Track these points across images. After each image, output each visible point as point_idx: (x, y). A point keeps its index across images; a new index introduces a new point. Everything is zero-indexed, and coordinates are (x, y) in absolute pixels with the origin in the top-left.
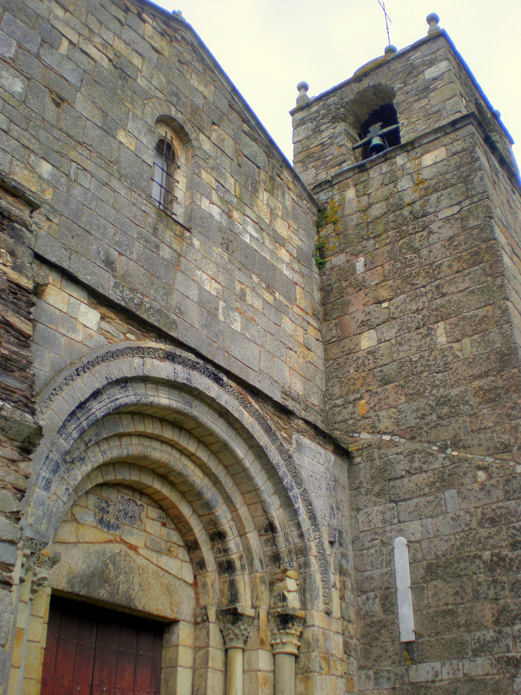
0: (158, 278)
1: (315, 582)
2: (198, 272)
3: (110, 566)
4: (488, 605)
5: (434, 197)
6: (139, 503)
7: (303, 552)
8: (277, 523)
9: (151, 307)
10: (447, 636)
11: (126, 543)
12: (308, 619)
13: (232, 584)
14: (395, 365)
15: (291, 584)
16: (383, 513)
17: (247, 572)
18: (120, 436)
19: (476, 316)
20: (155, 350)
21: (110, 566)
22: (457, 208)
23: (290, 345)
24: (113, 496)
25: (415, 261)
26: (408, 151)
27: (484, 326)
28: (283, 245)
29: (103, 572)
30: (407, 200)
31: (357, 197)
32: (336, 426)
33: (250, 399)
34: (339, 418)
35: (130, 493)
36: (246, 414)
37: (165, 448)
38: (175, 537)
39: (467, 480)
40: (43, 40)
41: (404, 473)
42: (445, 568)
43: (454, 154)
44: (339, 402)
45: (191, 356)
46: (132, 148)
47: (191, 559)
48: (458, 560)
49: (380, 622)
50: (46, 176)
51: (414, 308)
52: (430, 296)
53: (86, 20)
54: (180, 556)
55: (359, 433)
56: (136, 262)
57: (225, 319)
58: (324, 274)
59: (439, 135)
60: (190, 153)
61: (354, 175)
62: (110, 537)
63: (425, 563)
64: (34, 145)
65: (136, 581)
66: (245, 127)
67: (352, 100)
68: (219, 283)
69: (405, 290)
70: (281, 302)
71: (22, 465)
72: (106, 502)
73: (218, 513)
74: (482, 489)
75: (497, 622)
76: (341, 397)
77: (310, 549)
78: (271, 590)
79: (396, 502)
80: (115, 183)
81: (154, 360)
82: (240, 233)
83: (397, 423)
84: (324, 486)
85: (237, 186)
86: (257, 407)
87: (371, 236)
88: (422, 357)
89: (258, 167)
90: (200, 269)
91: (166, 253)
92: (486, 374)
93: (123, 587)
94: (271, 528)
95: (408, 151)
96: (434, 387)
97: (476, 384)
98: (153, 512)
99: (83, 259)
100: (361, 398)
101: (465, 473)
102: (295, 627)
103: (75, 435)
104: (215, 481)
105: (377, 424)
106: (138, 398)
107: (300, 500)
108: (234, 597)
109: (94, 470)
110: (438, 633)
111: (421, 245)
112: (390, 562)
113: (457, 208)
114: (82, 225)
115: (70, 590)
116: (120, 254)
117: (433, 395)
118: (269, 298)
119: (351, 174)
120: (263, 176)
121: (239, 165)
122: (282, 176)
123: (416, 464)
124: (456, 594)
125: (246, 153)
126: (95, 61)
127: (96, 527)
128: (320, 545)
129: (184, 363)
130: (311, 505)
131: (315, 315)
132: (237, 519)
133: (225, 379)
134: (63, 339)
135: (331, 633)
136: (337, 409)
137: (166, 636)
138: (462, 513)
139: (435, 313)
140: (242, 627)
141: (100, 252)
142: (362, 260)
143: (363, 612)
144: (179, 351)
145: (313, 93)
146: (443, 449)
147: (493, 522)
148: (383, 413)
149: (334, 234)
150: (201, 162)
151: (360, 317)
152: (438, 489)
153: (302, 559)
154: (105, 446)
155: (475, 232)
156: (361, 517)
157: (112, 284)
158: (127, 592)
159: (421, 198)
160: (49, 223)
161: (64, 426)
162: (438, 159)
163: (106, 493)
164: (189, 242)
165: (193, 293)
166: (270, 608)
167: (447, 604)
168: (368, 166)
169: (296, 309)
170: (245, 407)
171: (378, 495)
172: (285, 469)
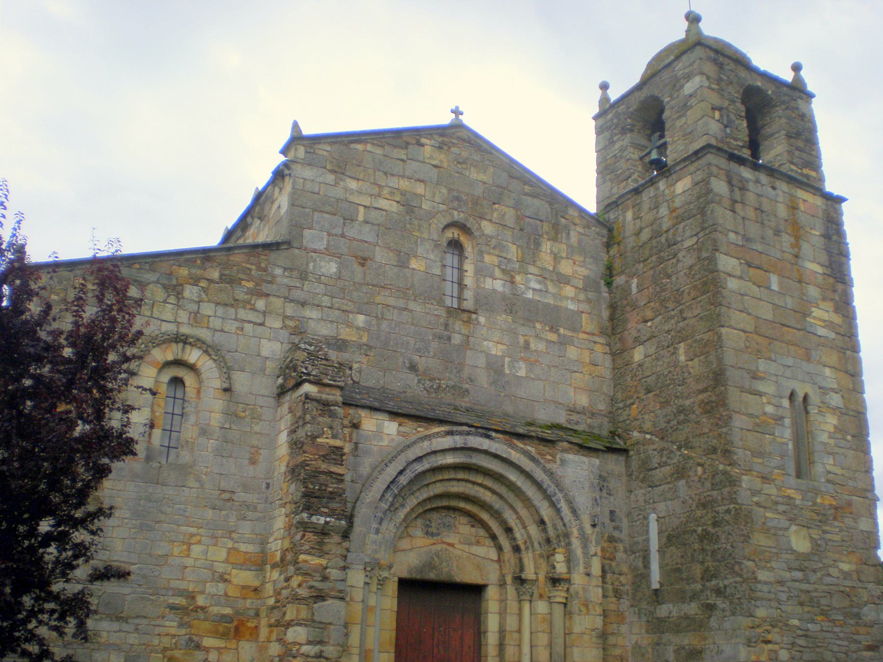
0: (451, 362)
1: (576, 555)
2: (485, 343)
3: (436, 559)
4: (699, 566)
5: (681, 226)
6: (453, 516)
7: (567, 535)
8: (546, 519)
9: (447, 386)
10: (677, 587)
11: (445, 543)
12: (572, 580)
13: (521, 560)
14: (654, 377)
15: (559, 557)
16: (645, 495)
17: (531, 551)
18: (428, 485)
19: (703, 339)
20: (438, 433)
21: (436, 559)
22: (695, 239)
23: (575, 369)
24: (435, 516)
25: (668, 286)
26: (667, 177)
27: (707, 349)
28: (568, 283)
29: (431, 563)
30: (664, 228)
31: (634, 219)
32: (619, 425)
33: (515, 441)
34: (621, 419)
35: (446, 511)
36: (513, 452)
37: (460, 483)
38: (482, 532)
39: (691, 473)
40: (345, 219)
41: (657, 465)
42: (677, 538)
43: (697, 184)
44: (621, 405)
45: (465, 428)
46: (422, 269)
47: (495, 545)
48: (685, 532)
49: (641, 574)
50: (361, 325)
51: (666, 328)
52: (676, 318)
53: (374, 180)
54: (487, 544)
55: (633, 431)
56: (433, 357)
57: (511, 371)
58: (612, 293)
59: (687, 163)
60: (474, 241)
61: (632, 196)
62: (433, 541)
63: (666, 533)
64: (350, 306)
65: (454, 565)
66: (527, 189)
67: (635, 110)
68: (504, 344)
69: (662, 312)
70: (565, 336)
71: (344, 544)
72: (429, 520)
73: (505, 517)
74: (699, 481)
75: (702, 578)
76: (622, 401)
77: (572, 533)
78: (548, 562)
79: (652, 487)
80: (412, 305)
81: (439, 439)
82: (523, 293)
83: (654, 425)
84: (587, 485)
85: (519, 250)
86: (521, 446)
87: (642, 259)
88: (670, 372)
89: (541, 221)
90: (486, 340)
91: (457, 339)
92: (705, 390)
93: (445, 570)
94: (542, 522)
95: (667, 177)
96: (677, 397)
97: (701, 397)
98: (464, 520)
99: (394, 372)
100: (633, 404)
101: (691, 468)
102: (562, 585)
103: (391, 499)
104: (501, 497)
105: (643, 426)
106: (431, 465)
107: (562, 501)
108: (522, 569)
109: (419, 504)
110: (671, 584)
111: (672, 272)
112: (647, 532)
113: (695, 239)
114: (390, 348)
115: (410, 577)
116: (420, 356)
117: (675, 404)
118: (553, 337)
119: (629, 196)
120: (546, 227)
121: (521, 230)
122: (567, 216)
123: (664, 459)
124: (682, 557)
125: (527, 214)
126: (386, 211)
127: (424, 537)
128: (581, 529)
129: (460, 433)
130: (571, 503)
131: (602, 333)
132: (519, 518)
133: (493, 434)
134: (375, 448)
135: (591, 588)
136: (620, 411)
137: (483, 594)
138: (687, 498)
139: (679, 334)
140: (527, 587)
141: (405, 362)
142: (635, 281)
143: (633, 567)
144: (455, 428)
145: (614, 94)
146: (679, 448)
147: (704, 506)
148: (646, 417)
149: (618, 255)
150: (484, 248)
151: (634, 333)
152: (676, 479)
153: (567, 540)
154: (418, 494)
155: (706, 263)
156: (633, 497)
157: (416, 381)
158: (449, 572)
159: (674, 226)
160: (368, 357)
161: (383, 496)
162: (686, 188)
163: (428, 516)
164: (475, 322)
165: (482, 361)
166: (547, 573)
167: (677, 564)
168: (641, 189)
169: (582, 336)
170: (512, 448)
171: (642, 481)
172: (549, 482)
